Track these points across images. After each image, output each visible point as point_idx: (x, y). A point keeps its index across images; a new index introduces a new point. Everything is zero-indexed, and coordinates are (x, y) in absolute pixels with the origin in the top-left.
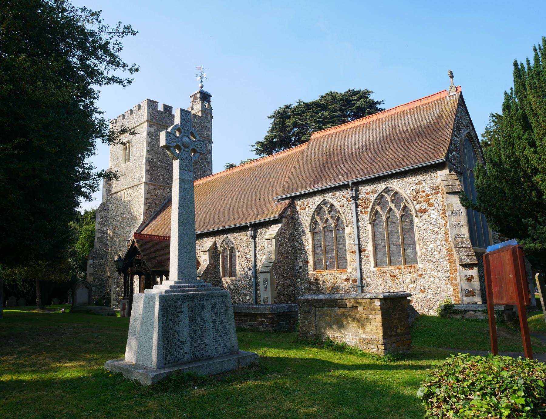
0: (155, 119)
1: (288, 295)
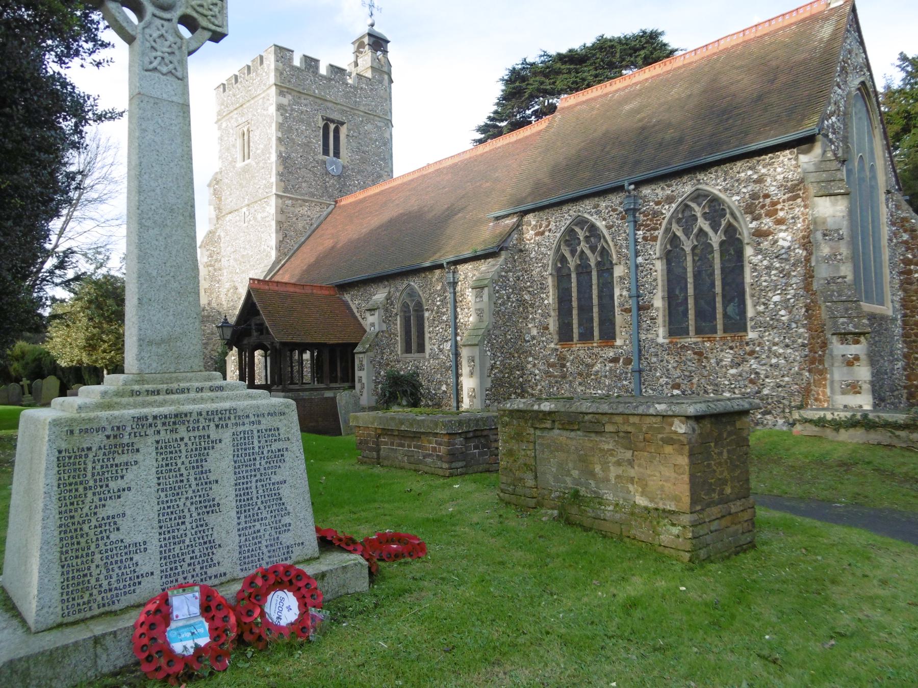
0: (289, 81)
1: (510, 384)
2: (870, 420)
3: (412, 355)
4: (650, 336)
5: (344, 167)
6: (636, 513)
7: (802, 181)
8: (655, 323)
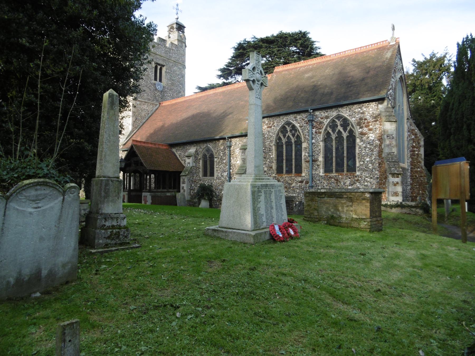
2: (403, 205)
3: (207, 178)
4: (316, 172)
5: (164, 87)
6: (353, 219)
7: (379, 115)
8: (319, 167)
